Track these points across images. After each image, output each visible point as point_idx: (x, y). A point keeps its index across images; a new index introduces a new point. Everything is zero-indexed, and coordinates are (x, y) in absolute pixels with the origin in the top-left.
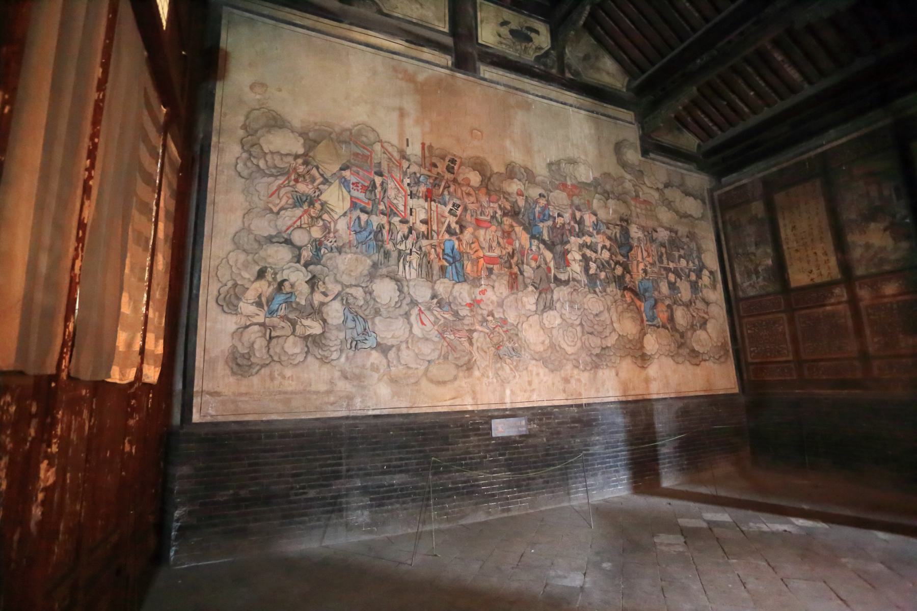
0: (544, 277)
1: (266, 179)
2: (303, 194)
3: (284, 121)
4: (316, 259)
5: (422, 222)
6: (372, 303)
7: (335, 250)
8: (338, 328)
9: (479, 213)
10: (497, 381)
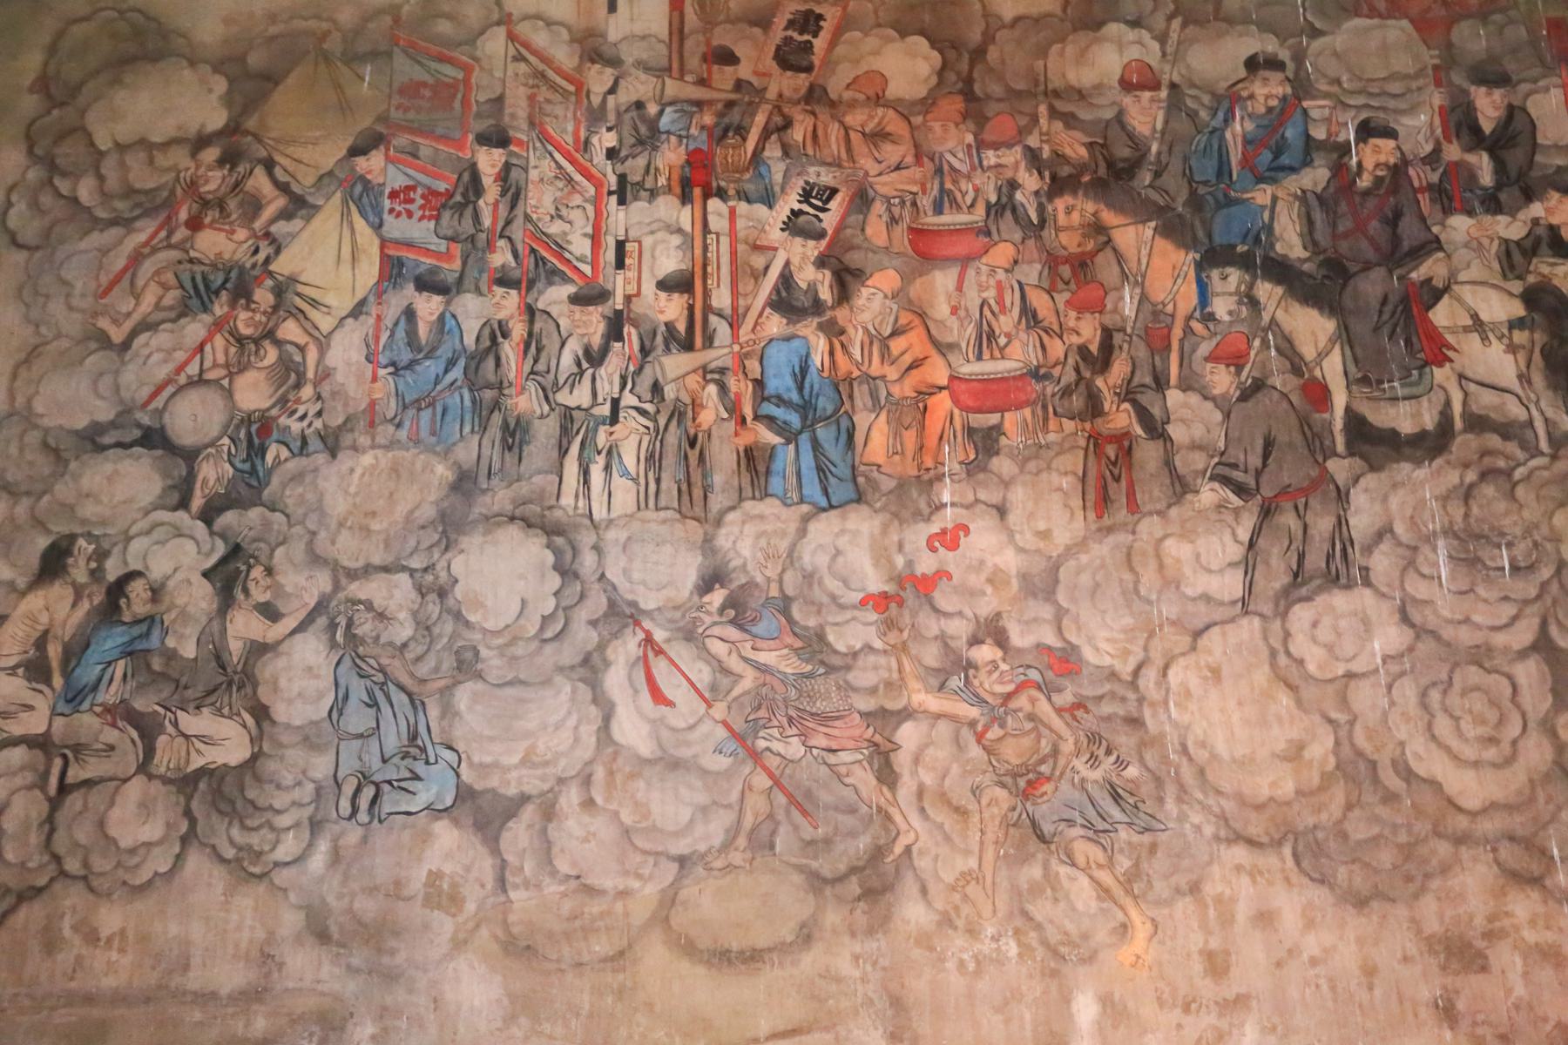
0: (1287, 433)
1: (96, 239)
2: (214, 266)
3: (164, 33)
4: (248, 487)
5: (664, 285)
6: (449, 627)
7: (315, 444)
8: (309, 740)
9: (925, 202)
10: (1025, 950)
